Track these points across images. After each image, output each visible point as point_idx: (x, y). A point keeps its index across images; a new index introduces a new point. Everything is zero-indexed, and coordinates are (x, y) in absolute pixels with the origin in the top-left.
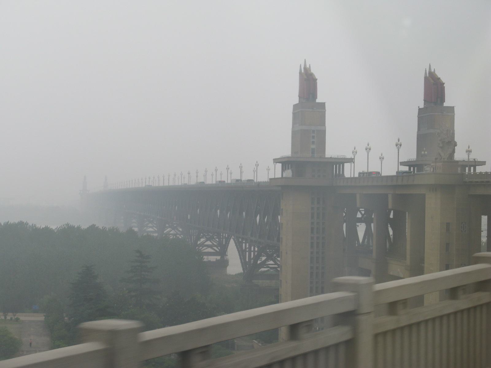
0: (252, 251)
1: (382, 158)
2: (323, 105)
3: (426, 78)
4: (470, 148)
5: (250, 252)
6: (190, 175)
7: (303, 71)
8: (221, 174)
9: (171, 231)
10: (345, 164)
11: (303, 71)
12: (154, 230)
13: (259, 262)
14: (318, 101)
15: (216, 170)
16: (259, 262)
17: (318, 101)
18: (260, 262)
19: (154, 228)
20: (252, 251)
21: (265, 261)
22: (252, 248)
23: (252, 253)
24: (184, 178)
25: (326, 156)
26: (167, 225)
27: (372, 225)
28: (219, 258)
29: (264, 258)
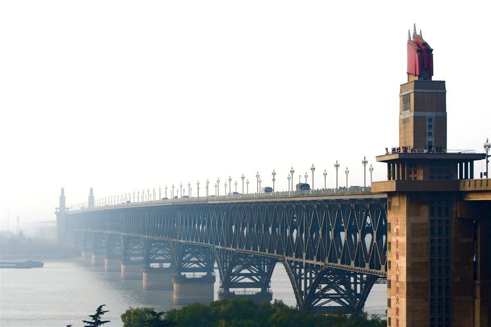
0: (308, 278)
1: (325, 174)
2: (442, 84)
3: (409, 43)
4: (338, 163)
5: (306, 279)
6: (259, 179)
7: (412, 40)
8: (236, 184)
9: (157, 250)
10: (475, 162)
11: (412, 40)
12: (140, 253)
13: (317, 291)
14: (434, 78)
15: (230, 180)
16: (317, 291)
17: (434, 78)
18: (319, 290)
19: (166, 256)
20: (308, 278)
21: (325, 289)
22: (308, 274)
23: (308, 281)
24: (184, 191)
25: (448, 152)
26: (153, 244)
27: (270, 228)
28: (259, 290)
29: (323, 286)
